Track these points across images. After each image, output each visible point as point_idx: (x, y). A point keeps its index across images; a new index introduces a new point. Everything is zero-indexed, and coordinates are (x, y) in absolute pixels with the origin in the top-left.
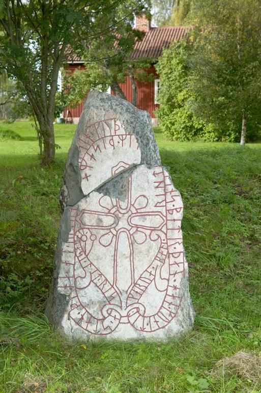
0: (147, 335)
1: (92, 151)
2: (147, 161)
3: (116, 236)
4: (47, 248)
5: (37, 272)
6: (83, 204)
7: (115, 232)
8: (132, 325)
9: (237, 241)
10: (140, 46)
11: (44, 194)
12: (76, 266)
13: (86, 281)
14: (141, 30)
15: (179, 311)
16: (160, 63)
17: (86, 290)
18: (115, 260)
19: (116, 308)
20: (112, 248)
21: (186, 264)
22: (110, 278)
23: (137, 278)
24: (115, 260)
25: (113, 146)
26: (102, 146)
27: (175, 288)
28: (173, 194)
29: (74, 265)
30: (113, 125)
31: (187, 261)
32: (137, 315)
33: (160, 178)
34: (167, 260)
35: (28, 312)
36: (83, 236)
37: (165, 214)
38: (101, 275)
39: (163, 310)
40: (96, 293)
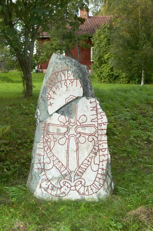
0: (86, 197)
2: (86, 94)
3: (68, 139)
5: (22, 160)
6: (49, 121)
7: (67, 137)
8: (78, 191)
9: (139, 142)
10: (82, 27)
13: (51, 165)
15: (105, 183)
16: (94, 37)
18: (68, 153)
21: (109, 156)
22: (65, 164)
23: (80, 163)
24: (68, 153)
25: (67, 86)
27: (103, 169)
28: (102, 114)
29: (44, 156)
32: (81, 185)
34: (98, 153)
36: (49, 139)
37: (97, 126)
38: (59, 162)
39: (96, 183)
40: (56, 172)
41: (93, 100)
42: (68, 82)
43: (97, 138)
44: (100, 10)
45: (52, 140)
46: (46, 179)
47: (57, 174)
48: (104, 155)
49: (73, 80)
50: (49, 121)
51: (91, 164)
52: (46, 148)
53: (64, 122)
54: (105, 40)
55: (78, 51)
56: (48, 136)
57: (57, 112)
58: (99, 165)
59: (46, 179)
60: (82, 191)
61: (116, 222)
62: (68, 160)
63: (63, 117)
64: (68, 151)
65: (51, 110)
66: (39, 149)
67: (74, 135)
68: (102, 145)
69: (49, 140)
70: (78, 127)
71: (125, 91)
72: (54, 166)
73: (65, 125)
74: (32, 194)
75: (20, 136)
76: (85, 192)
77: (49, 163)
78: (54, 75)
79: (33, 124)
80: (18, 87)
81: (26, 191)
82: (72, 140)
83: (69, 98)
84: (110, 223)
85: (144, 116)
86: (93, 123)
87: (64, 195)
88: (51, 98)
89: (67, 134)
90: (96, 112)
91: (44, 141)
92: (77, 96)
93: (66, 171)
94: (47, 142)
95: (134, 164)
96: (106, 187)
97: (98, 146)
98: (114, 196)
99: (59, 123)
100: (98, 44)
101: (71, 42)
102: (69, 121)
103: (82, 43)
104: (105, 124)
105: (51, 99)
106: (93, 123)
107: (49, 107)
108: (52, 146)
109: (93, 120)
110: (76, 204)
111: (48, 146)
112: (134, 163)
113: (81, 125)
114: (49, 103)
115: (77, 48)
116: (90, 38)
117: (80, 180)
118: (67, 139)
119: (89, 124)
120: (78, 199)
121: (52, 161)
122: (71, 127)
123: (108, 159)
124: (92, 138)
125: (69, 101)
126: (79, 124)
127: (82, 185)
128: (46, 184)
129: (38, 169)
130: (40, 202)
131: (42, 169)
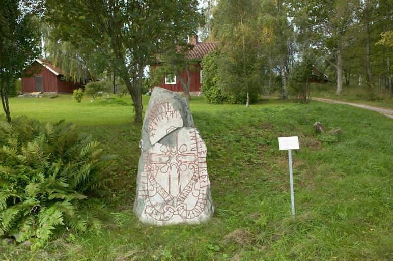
0: (188, 221)
1: (155, 121)
2: (185, 125)
3: (170, 167)
4: (135, 172)
5: (130, 185)
6: (151, 151)
7: (169, 165)
8: (181, 216)
9: (241, 163)
10: (191, 52)
11: (134, 141)
13: (154, 192)
14: (50, 189)
15: (206, 207)
16: (202, 61)
17: (154, 197)
18: (170, 180)
19: (170, 206)
20: (168, 174)
21: (209, 182)
22: (168, 191)
23: (182, 190)
24: (170, 180)
26: (161, 118)
27: (203, 194)
28: (201, 143)
30: (167, 106)
31: (210, 179)
32: (183, 210)
33: (193, 134)
34: (198, 180)
35: (124, 209)
37: (197, 154)
38: (162, 189)
39: (197, 207)
40: (160, 199)
41: (192, 130)
44: (208, 36)
47: (160, 200)
50: (151, 151)
53: (166, 151)
54: (213, 64)
55: (188, 74)
56: (150, 165)
57: (159, 142)
60: (184, 215)
61: (214, 245)
64: (170, 179)
65: (153, 140)
66: (143, 178)
69: (152, 169)
71: (231, 114)
74: (138, 219)
75: (128, 162)
79: (138, 151)
80: (128, 111)
81: (132, 216)
82: (174, 168)
84: (208, 246)
85: (247, 138)
86: (193, 152)
87: (168, 219)
92: (177, 127)
93: (169, 197)
95: (236, 185)
96: (207, 211)
98: (214, 218)
99: (161, 153)
100: (206, 67)
101: (181, 66)
103: (192, 67)
106: (193, 152)
107: (151, 138)
110: (178, 228)
112: (235, 185)
114: (151, 134)
115: (187, 71)
116: (199, 62)
120: (180, 223)
122: (172, 156)
129: (143, 196)
130: (145, 226)
131: (146, 195)
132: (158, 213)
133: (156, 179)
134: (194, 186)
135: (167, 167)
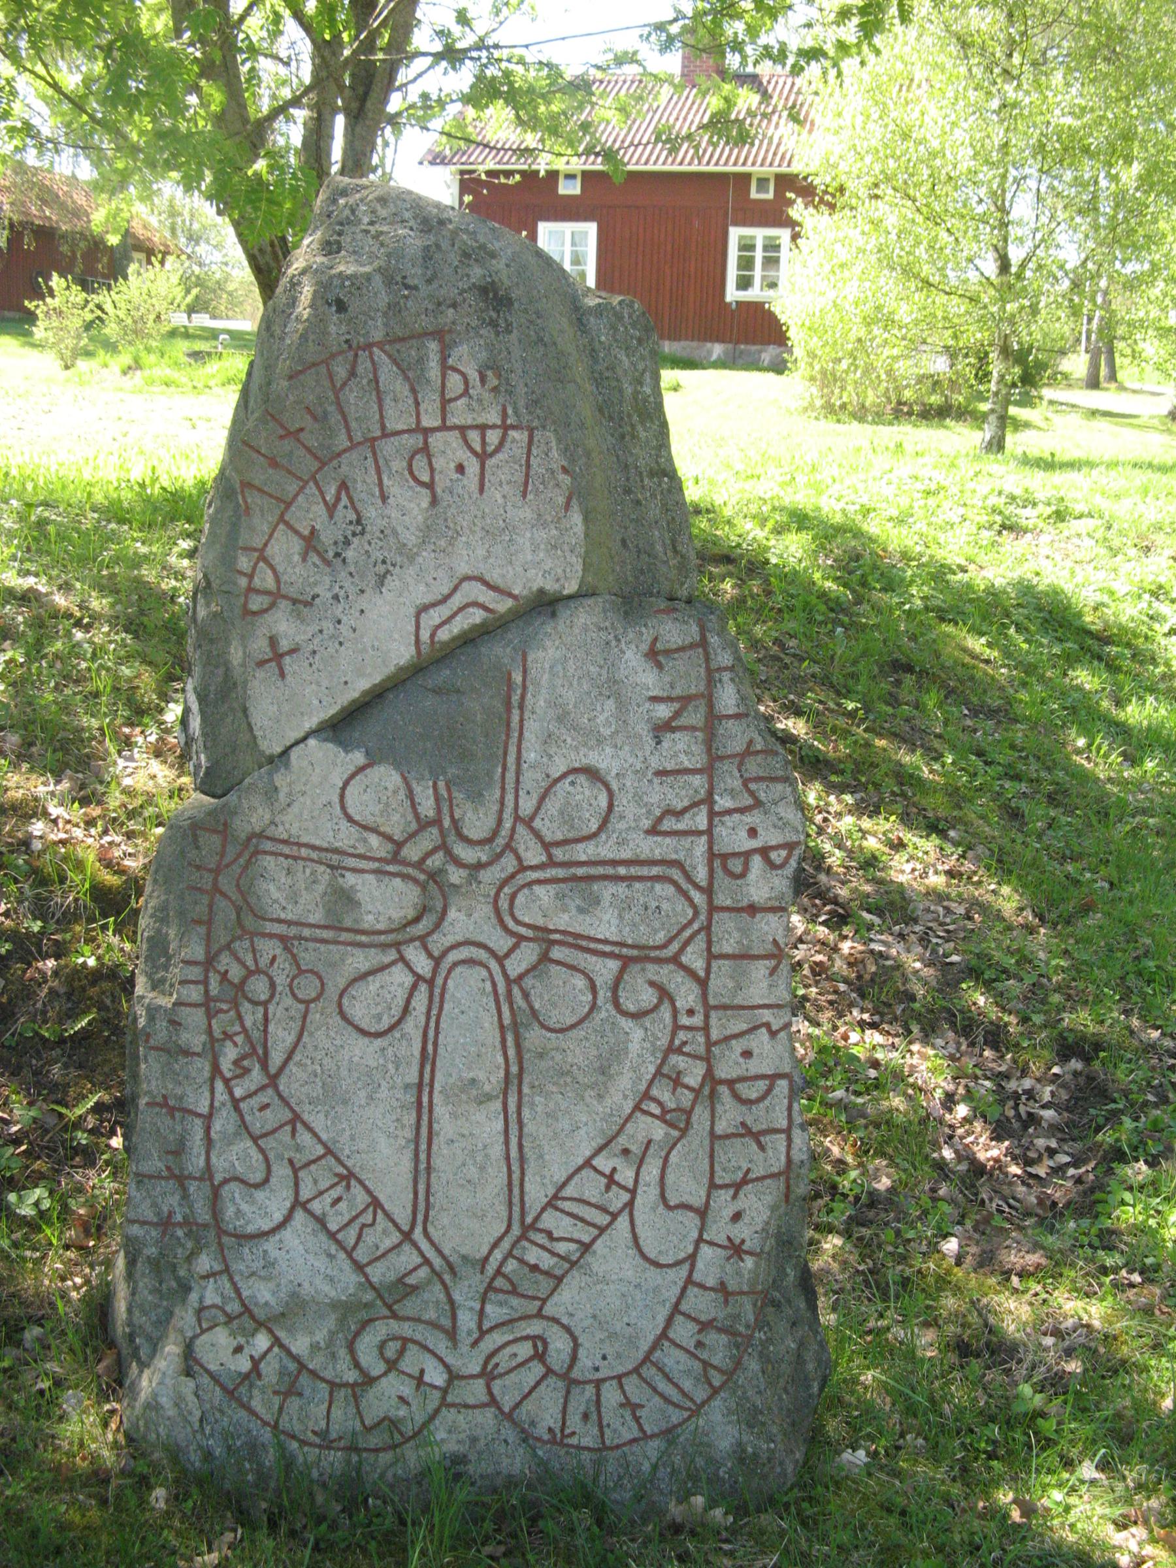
7: (423, 965)
12: (217, 1126)
13: (275, 1203)
17: (270, 1245)
23: (536, 1194)
25: (430, 486)
28: (753, 767)
29: (208, 1118)
32: (537, 1369)
34: (701, 1115)
36: (250, 973)
37: (701, 875)
38: (348, 1178)
40: (321, 1263)
42: (449, 450)
43: (703, 983)
45: (281, 980)
46: (234, 1307)
48: (756, 1136)
49: (493, 437)
51: (630, 1204)
52: (229, 1054)
53: (396, 825)
58: (703, 1213)
59: (234, 1307)
62: (423, 1166)
63: (387, 777)
64: (422, 1087)
67: (482, 955)
68: (738, 1046)
69: (259, 987)
70: (521, 879)
72: (299, 1215)
73: (521, 829)
76: (574, 1421)
77: (257, 1186)
78: (309, 378)
82: (467, 990)
83: (457, 601)
88: (276, 596)
89: (423, 939)
90: (698, 749)
91: (214, 987)
94: (236, 1006)
97: (702, 1050)
102: (447, 823)
104: (777, 856)
105: (283, 604)
108: (281, 1037)
109: (668, 824)
111: (248, 1038)
113: (552, 863)
117: (535, 1328)
118: (423, 987)
119: (626, 854)
121: (281, 1171)
123: (789, 1161)
124: (652, 984)
125: (444, 635)
126: (533, 855)
127: (549, 1371)
128: (238, 1349)
132: (304, 1380)
133: (294, 1083)
134: (651, 1171)
135: (400, 978)
